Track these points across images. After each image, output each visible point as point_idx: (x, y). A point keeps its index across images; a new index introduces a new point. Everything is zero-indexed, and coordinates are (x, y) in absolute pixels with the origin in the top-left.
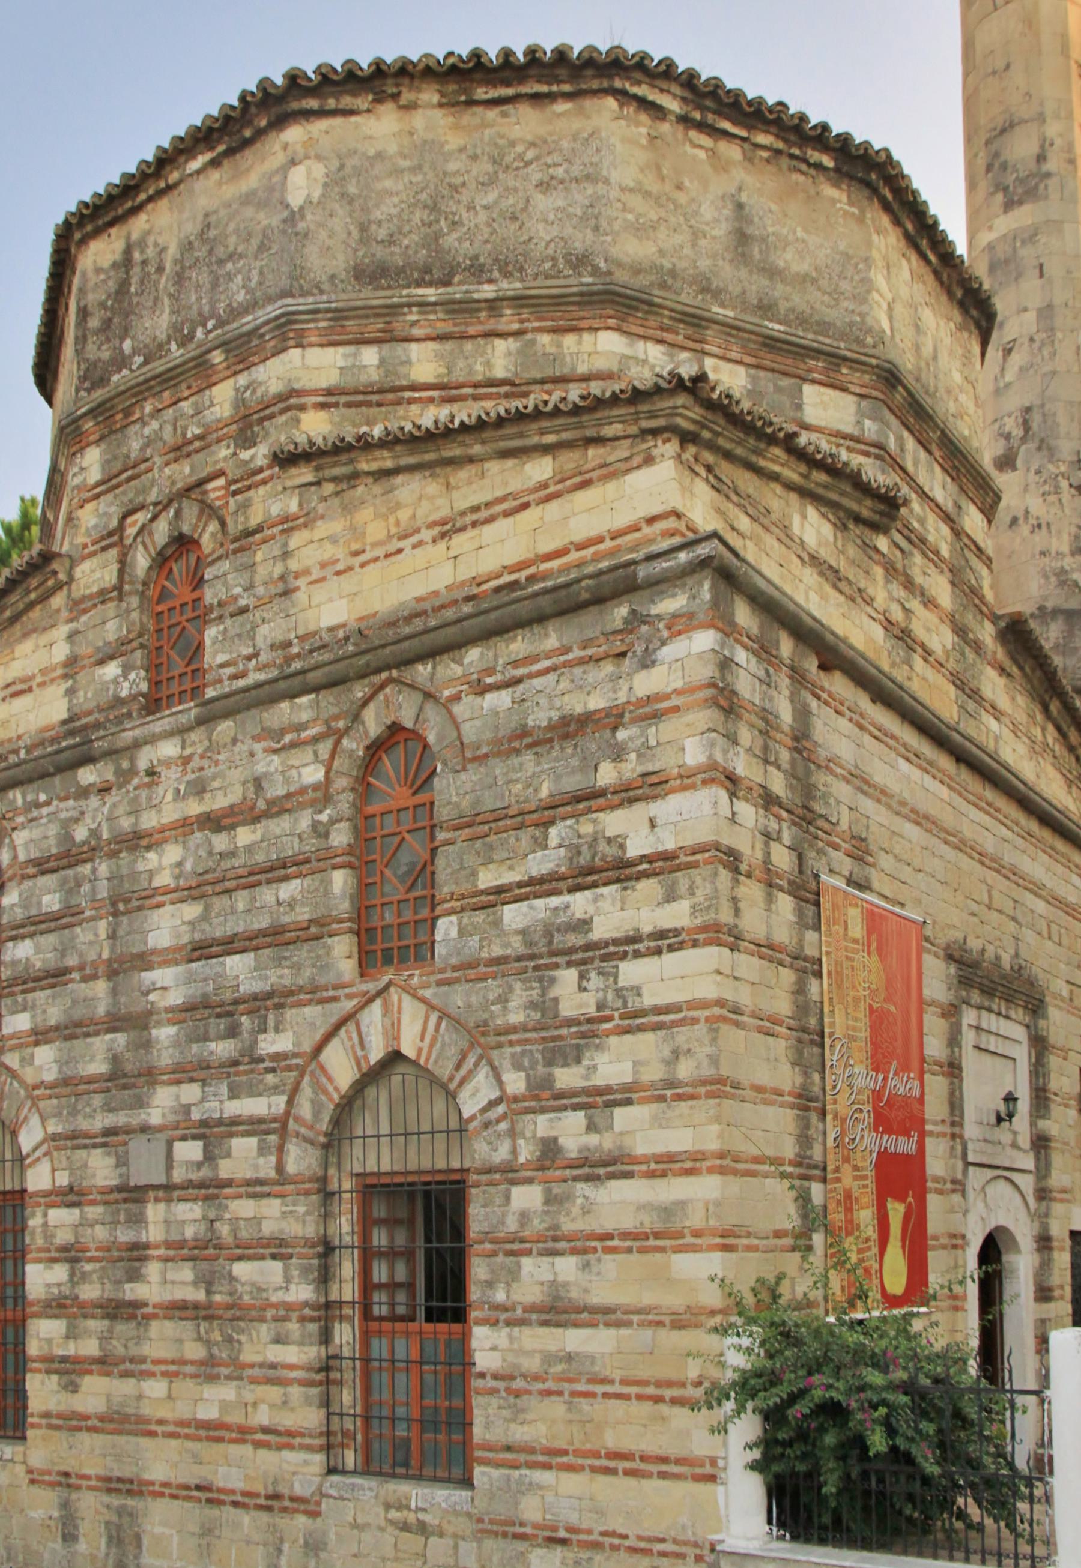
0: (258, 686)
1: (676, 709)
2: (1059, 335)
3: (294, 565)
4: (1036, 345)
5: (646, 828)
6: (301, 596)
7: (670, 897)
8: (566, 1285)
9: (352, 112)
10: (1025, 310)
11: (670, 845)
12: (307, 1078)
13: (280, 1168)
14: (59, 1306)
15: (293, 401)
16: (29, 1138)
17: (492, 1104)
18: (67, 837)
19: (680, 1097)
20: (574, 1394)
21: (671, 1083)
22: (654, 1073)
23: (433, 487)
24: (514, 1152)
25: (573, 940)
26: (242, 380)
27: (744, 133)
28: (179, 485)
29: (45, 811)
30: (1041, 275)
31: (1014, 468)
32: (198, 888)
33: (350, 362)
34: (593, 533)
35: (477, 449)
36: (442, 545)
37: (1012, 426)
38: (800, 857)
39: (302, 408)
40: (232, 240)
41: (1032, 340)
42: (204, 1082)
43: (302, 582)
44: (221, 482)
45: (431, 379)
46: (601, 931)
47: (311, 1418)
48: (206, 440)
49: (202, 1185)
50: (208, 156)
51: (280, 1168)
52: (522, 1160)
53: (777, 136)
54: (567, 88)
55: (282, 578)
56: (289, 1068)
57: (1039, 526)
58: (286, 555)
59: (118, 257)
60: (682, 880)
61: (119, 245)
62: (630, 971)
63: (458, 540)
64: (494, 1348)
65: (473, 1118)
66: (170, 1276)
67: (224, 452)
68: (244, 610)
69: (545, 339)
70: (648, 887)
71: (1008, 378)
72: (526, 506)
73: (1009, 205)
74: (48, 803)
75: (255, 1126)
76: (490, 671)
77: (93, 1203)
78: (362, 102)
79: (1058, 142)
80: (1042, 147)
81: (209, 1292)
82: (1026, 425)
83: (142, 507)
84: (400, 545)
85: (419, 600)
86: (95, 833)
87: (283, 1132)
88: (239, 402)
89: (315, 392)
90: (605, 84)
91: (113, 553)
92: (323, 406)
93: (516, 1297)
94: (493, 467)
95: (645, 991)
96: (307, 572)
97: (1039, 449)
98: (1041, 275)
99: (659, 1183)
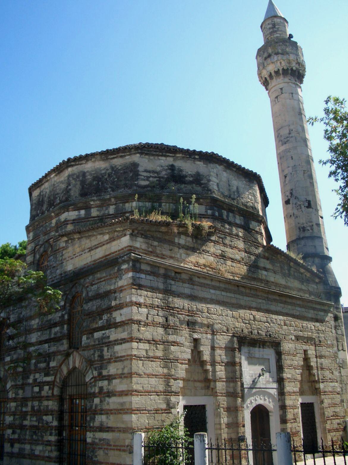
0: (56, 283)
1: (125, 289)
2: (298, 172)
3: (64, 257)
4: (292, 175)
5: (119, 316)
6: (64, 264)
7: (124, 331)
8: (103, 422)
9: (82, 164)
10: (289, 167)
11: (124, 319)
12: (58, 373)
13: (53, 393)
14: (10, 426)
15: (65, 223)
16: (9, 386)
17: (92, 378)
18: (19, 317)
19: (125, 377)
20: (104, 449)
21: (123, 374)
22: (120, 372)
23: (88, 241)
24: (95, 390)
25: (107, 341)
26: (57, 218)
27: (174, 155)
28: (45, 240)
29: (16, 311)
30: (292, 159)
31: (290, 204)
32: (40, 329)
33: (78, 214)
34: (115, 250)
35: (95, 233)
36: (89, 253)
37: (288, 194)
38: (167, 319)
39: (67, 224)
40: (58, 191)
41: (291, 174)
42: (40, 373)
43: (65, 261)
44: (52, 240)
45: (96, 215)
46: (112, 338)
47: (54, 454)
48: (50, 231)
49: (38, 397)
50: (55, 174)
51: (53, 393)
52: (96, 392)
53: (183, 154)
54: (128, 153)
55: (62, 260)
56: (55, 370)
57: (297, 217)
58: (62, 255)
59: (38, 194)
60: (126, 327)
61: (39, 192)
62: (117, 348)
63: (92, 252)
64: (90, 437)
65: (88, 382)
66: (32, 419)
67: (53, 233)
68: (54, 267)
69: (121, 205)
70: (120, 329)
71: (286, 182)
72: (104, 245)
73: (282, 145)
74: (16, 309)
75: (48, 383)
76: (94, 281)
77: (18, 401)
78: (84, 162)
79: (294, 130)
80: (290, 131)
81: (39, 423)
82: (291, 193)
83: (38, 245)
84: (82, 253)
85: (85, 264)
86: (23, 316)
87: (54, 385)
88: (56, 223)
89: (71, 220)
90: (137, 152)
91: (32, 255)
92: (72, 223)
93: (95, 425)
94: (99, 237)
95: (119, 353)
96: (65, 259)
97: (295, 199)
98: (292, 159)
99: (121, 398)
